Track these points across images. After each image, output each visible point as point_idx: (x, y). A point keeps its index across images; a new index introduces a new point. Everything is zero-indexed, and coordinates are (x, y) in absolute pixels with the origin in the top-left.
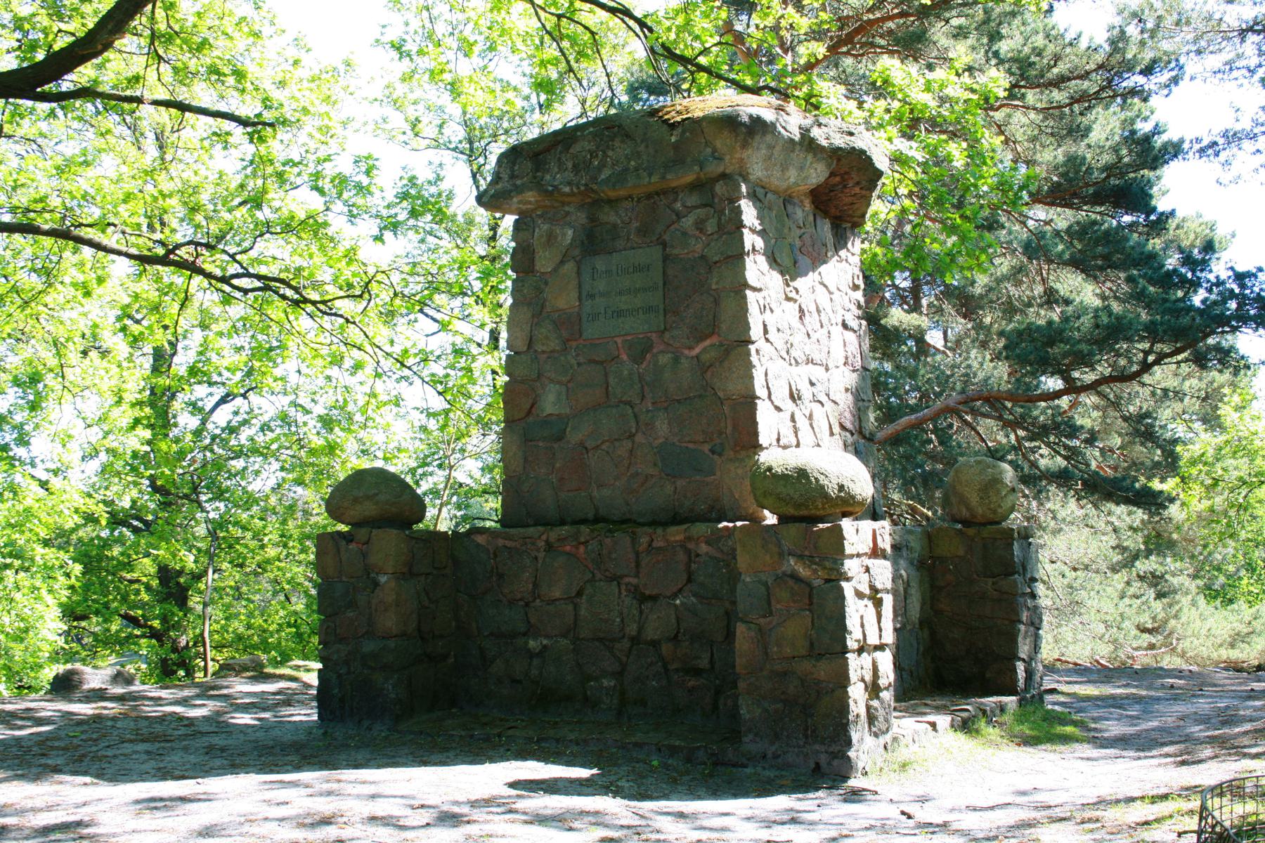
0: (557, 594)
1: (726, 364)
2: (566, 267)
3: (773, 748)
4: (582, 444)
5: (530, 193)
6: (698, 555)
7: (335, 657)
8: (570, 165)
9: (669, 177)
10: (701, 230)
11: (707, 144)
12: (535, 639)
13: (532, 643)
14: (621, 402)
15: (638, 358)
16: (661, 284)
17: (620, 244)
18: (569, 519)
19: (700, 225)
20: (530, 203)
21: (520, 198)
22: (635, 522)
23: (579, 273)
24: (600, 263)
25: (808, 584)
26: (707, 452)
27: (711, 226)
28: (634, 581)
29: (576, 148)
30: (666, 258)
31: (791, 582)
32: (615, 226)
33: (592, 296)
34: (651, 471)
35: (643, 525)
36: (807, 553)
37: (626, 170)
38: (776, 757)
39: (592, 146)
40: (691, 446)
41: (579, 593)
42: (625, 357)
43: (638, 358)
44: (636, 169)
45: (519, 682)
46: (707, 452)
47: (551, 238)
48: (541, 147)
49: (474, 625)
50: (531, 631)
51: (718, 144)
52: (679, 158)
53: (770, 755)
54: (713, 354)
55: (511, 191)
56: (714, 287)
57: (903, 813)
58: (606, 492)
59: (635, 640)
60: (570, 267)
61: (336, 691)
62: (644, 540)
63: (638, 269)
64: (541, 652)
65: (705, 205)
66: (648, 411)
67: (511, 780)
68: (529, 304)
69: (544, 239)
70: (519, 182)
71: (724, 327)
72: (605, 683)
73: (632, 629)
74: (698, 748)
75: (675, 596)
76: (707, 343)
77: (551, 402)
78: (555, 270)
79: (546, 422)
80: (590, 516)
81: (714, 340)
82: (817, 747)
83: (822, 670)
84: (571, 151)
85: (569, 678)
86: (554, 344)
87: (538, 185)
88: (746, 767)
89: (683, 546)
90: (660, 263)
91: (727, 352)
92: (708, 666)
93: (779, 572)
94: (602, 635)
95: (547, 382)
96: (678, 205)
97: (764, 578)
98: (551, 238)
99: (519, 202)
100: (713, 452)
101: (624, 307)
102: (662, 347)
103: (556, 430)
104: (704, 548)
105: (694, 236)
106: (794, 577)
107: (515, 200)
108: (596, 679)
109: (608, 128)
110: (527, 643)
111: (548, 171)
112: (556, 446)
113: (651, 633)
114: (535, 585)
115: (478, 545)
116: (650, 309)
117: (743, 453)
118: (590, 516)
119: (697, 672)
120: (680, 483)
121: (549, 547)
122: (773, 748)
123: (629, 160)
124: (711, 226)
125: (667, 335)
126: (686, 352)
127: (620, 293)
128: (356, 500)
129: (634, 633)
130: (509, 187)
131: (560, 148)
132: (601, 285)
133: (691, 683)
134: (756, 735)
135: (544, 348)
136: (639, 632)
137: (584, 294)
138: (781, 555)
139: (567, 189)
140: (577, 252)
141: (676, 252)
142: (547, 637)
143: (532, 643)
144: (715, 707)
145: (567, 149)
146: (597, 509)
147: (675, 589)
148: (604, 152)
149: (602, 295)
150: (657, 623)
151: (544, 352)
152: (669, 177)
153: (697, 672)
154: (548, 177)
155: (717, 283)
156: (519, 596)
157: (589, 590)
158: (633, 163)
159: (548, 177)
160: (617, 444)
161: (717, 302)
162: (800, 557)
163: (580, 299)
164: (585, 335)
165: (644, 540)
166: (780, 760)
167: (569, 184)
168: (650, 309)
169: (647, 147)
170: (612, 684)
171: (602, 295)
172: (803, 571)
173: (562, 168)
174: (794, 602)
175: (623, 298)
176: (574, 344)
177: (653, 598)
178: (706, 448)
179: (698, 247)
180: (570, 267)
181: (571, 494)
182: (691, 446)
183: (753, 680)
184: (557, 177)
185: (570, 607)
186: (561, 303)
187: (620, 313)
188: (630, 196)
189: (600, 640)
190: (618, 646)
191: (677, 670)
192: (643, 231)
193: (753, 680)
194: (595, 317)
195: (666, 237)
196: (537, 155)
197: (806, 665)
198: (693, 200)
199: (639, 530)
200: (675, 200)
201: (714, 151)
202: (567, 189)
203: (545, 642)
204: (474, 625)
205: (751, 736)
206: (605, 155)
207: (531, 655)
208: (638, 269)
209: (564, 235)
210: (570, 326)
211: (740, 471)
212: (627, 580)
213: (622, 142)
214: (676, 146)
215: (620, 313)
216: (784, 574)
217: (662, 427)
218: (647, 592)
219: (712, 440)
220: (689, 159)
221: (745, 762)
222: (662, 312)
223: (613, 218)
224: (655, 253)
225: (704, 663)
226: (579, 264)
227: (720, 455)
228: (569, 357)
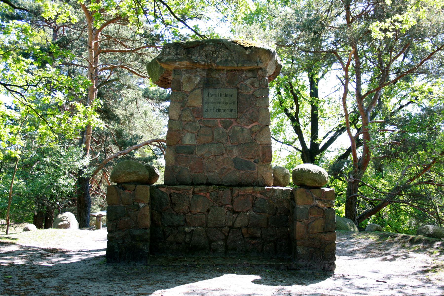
0: (199, 211)
1: (261, 132)
2: (197, 91)
3: (309, 263)
4: (202, 156)
5: (186, 62)
6: (257, 198)
7: (117, 237)
8: (204, 54)
9: (245, 65)
10: (253, 86)
11: (259, 57)
12: (188, 227)
13: (187, 229)
14: (218, 142)
15: (226, 127)
16: (236, 102)
17: (219, 86)
18: (195, 183)
19: (252, 84)
20: (184, 65)
21: (180, 63)
22: (223, 185)
23: (202, 94)
24: (211, 91)
25: (322, 209)
26: (252, 162)
27: (256, 85)
28: (230, 206)
29: (206, 49)
30: (238, 93)
31: (317, 208)
32: (217, 79)
33: (207, 103)
34: (231, 167)
35: (235, 186)
36: (322, 199)
37: (227, 60)
38: (310, 266)
39: (213, 49)
40: (247, 159)
41: (208, 211)
42: (220, 126)
43: (226, 127)
44: (231, 61)
45: (181, 243)
46: (252, 162)
47: (190, 79)
48: (191, 46)
49: (160, 222)
50: (187, 224)
51: (262, 58)
52: (249, 59)
53: (308, 265)
54: (257, 129)
55: (176, 60)
56: (257, 106)
57: (386, 282)
58: (211, 174)
59: (231, 227)
60: (198, 91)
61: (118, 250)
62: (236, 192)
63: (227, 95)
64: (190, 232)
65: (254, 78)
66: (230, 146)
67: (253, 280)
68: (179, 102)
69: (187, 79)
70: (179, 57)
71: (260, 120)
72: (219, 243)
73: (230, 223)
74: (281, 265)
75: (247, 212)
76: (254, 124)
77: (188, 140)
78: (191, 91)
79: (185, 147)
80: (205, 182)
81: (256, 124)
82: (325, 262)
83: (328, 237)
84: (204, 49)
85: (203, 241)
86: (191, 118)
87: (190, 59)
88: (300, 270)
89: (251, 195)
90: (236, 95)
91: (262, 129)
92: (260, 236)
93: (312, 205)
94: (217, 226)
95: (186, 132)
96: (243, 76)
97: (307, 207)
98: (190, 79)
99: (179, 64)
100: (255, 162)
101: (221, 108)
102: (236, 124)
103: (190, 150)
104: (259, 195)
105: (250, 87)
106: (317, 206)
107: (177, 63)
108: (215, 241)
109: (219, 44)
110: (184, 229)
111: (194, 55)
112: (190, 156)
113: (237, 225)
114: (189, 207)
115: (162, 192)
116: (232, 110)
117: (266, 163)
118: (205, 182)
119: (255, 238)
120: (242, 172)
121: (194, 193)
122: (309, 263)
123: (228, 57)
124: (256, 85)
125: (238, 120)
126: (246, 127)
127: (220, 103)
128: (129, 173)
129: (231, 225)
130: (175, 58)
131: (199, 48)
132: (212, 99)
133: (254, 242)
134: (303, 259)
135: (186, 119)
136: (234, 223)
137: (204, 102)
138: (313, 199)
139: (203, 63)
140: (201, 86)
141: (242, 92)
142: (193, 227)
143: (187, 229)
144: (262, 250)
145: (202, 48)
146: (207, 180)
147: (247, 209)
148: (219, 52)
149: (212, 103)
150: (240, 222)
151: (185, 121)
152: (245, 65)
153: (255, 238)
154: (194, 57)
155: (258, 105)
156: (182, 211)
157: (212, 210)
158: (229, 58)
159: (194, 57)
160: (217, 157)
161: (258, 111)
162: (320, 200)
163: (203, 103)
164: (204, 117)
165: (236, 192)
166: (312, 267)
167: (204, 61)
168: (232, 110)
169: (235, 53)
170: (222, 243)
171: (212, 103)
172: (321, 205)
173: (200, 54)
174: (318, 215)
175: (221, 105)
176: (199, 119)
177: (238, 213)
178: (252, 161)
179: (251, 91)
180: (198, 91)
181: (196, 174)
182: (247, 159)
183: (303, 241)
184: (198, 57)
185: (204, 216)
186: (195, 104)
187: (219, 110)
188: (224, 69)
189: (216, 227)
190: (224, 229)
191: (247, 238)
192: (229, 82)
193: (303, 241)
194: (209, 110)
195: (238, 86)
196: (188, 48)
197: (322, 235)
198: (249, 75)
199: (234, 188)
200: (243, 74)
201: (260, 59)
202: (203, 63)
203: (192, 228)
204: (160, 222)
205: (301, 260)
206: (219, 54)
207: (186, 233)
208: (227, 95)
209: (196, 79)
210: (198, 113)
211: (265, 169)
212: (227, 206)
213: (225, 50)
214: (248, 56)
215: (219, 110)
216: (314, 206)
217: (236, 152)
218: (236, 211)
219: (255, 158)
220: (253, 61)
221: (299, 268)
222: (236, 112)
223: (217, 76)
224: (235, 91)
225: (258, 235)
226: (202, 90)
227: (257, 163)
228: (197, 124)
